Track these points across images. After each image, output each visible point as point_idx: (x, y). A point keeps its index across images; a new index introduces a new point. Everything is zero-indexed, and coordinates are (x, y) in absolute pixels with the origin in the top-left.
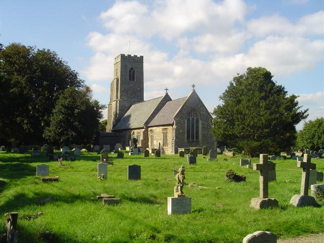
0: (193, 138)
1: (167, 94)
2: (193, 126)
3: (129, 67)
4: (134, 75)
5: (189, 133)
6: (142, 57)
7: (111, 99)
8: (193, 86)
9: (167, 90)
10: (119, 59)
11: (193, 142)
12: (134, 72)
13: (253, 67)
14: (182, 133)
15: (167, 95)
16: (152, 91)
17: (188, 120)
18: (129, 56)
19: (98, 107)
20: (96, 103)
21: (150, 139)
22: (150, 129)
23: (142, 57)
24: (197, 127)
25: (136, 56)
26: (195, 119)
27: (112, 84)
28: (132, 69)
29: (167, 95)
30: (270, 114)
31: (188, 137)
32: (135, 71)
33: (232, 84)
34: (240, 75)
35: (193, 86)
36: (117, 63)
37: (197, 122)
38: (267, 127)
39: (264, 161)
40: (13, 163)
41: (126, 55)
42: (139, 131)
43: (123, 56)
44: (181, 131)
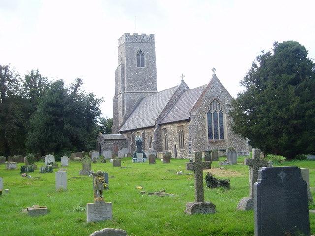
0: (216, 136)
1: (183, 81)
2: (216, 122)
3: (137, 49)
4: (143, 60)
5: (211, 133)
6: (152, 36)
7: (116, 92)
8: (214, 70)
9: (182, 76)
10: (123, 41)
11: (216, 142)
12: (143, 55)
13: (280, 41)
14: (202, 131)
15: (183, 83)
16: (166, 80)
17: (209, 113)
18: (136, 35)
19: (95, 103)
20: (91, 97)
21: (164, 140)
22: (163, 127)
23: (152, 36)
24: (222, 123)
25: (144, 35)
26: (213, 113)
27: (116, 73)
28: (140, 51)
29: (183, 83)
30: (302, 102)
31: (210, 136)
32: (145, 55)
33: (255, 65)
34: (265, 53)
35: (214, 70)
36: (121, 45)
37: (221, 116)
38: (297, 117)
39: (255, 157)
40: (102, 230)
41: (132, 34)
42: (150, 131)
43: (127, 36)
44: (200, 128)
